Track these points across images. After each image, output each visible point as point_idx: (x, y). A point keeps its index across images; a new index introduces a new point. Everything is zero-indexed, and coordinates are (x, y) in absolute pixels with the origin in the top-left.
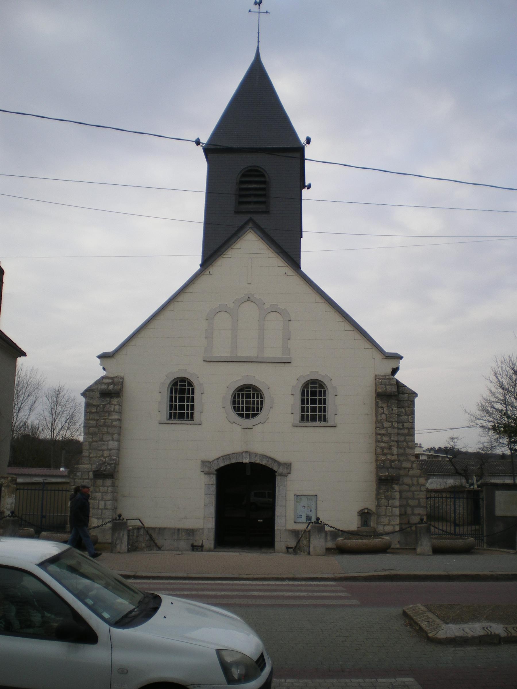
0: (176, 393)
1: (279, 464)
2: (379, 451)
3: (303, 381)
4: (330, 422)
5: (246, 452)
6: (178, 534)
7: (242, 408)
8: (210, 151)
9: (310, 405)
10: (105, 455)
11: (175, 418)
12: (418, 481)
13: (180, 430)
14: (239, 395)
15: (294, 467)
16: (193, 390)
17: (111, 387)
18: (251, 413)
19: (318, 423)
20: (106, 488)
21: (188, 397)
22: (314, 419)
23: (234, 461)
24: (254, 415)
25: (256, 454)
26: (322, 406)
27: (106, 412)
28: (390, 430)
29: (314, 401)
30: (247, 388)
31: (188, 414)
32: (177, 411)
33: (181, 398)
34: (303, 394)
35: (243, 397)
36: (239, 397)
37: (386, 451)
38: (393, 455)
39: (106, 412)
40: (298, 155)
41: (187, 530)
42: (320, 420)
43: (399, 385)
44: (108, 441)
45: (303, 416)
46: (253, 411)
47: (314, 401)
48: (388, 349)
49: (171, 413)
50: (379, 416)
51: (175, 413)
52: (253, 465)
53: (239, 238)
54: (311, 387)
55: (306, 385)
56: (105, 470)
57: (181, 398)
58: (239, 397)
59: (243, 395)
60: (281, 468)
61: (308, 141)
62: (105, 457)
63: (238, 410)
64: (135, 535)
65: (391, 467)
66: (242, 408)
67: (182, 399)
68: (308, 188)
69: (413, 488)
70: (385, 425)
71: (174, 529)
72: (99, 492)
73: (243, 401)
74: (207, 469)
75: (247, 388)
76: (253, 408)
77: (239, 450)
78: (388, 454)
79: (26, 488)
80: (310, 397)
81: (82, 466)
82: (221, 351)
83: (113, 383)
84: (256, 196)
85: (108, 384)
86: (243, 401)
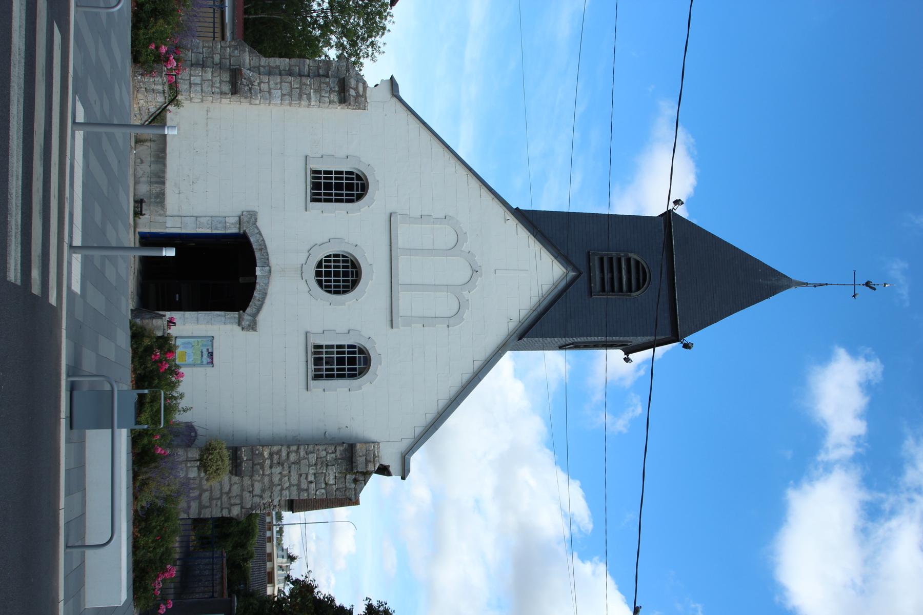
0: (347, 179)
1: (255, 315)
2: (275, 448)
3: (368, 346)
4: (313, 383)
5: (270, 271)
6: (157, 183)
7: (329, 267)
8: (668, 215)
9: (335, 356)
10: (262, 85)
11: (313, 178)
12: (235, 483)
13: (300, 186)
14: (347, 261)
15: (251, 334)
16: (351, 201)
17: (352, 92)
18: (323, 278)
19: (311, 367)
20: (218, 85)
21: (342, 195)
22: (318, 361)
23: (258, 255)
24: (320, 283)
25: (267, 284)
26: (334, 197)
27: (320, 86)
28: (304, 462)
29: (343, 362)
30: (357, 272)
31: (320, 194)
32: (323, 181)
33: (339, 187)
34: (350, 346)
35: (344, 267)
36: (344, 261)
37: (276, 457)
38: (271, 467)
39: (320, 86)
40: (669, 336)
41: (164, 194)
42: (315, 370)
43: (366, 475)
44: (281, 88)
45: (321, 347)
46: (326, 281)
47: (340, 361)
48: (415, 460)
49: (319, 172)
50: (323, 447)
51: (320, 178)
52: (252, 286)
53: (556, 258)
54: (360, 358)
55: (362, 351)
56: (241, 84)
57: (339, 187)
58: (344, 261)
59: (347, 267)
60: (249, 318)
61: (687, 346)
62: (259, 84)
63: (326, 261)
64: (156, 87)
65: (254, 465)
66: (329, 267)
67: (339, 187)
68: (625, 359)
69: (225, 498)
70: (311, 456)
71: (164, 177)
72: (212, 76)
73: (338, 267)
74: (245, 219)
75: (357, 272)
76: (330, 281)
77: (273, 261)
78: (272, 461)
79: (216, 20)
80: (346, 356)
81: (247, 54)
82: (405, 235)
83: (358, 95)
84: (612, 279)
85: (356, 89)
86: (338, 267)
